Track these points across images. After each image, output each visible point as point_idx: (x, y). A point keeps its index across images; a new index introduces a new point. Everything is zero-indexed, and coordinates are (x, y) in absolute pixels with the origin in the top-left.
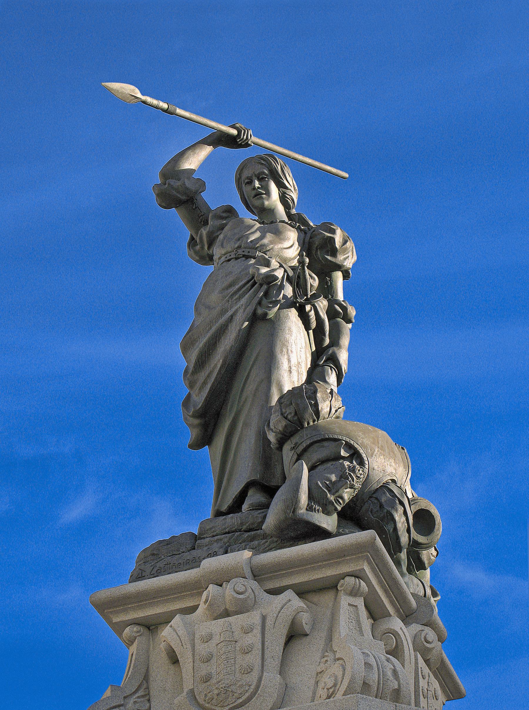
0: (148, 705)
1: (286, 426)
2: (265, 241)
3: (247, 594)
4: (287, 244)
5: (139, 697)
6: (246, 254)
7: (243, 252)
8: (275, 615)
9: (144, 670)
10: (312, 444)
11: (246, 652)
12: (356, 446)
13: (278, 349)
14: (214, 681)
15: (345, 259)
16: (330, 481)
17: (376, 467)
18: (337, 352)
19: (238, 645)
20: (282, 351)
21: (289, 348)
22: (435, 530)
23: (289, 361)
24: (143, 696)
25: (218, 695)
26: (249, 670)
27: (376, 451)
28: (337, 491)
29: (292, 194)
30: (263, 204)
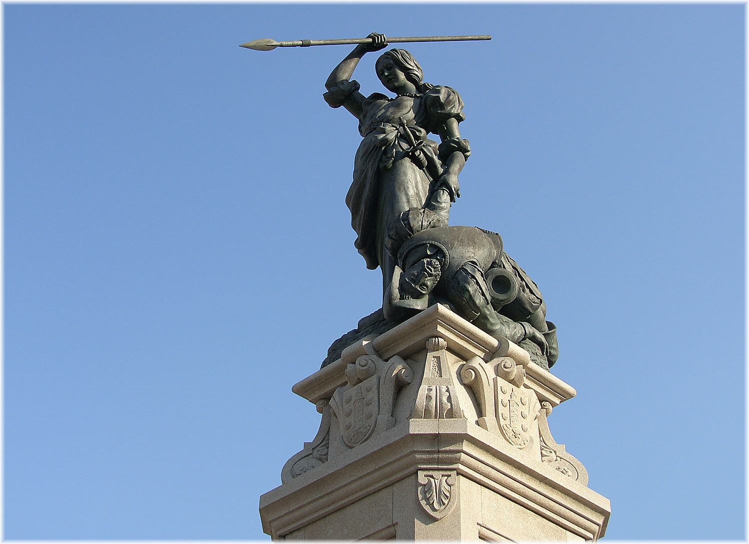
0: (327, 450)
1: (392, 244)
2: (388, 114)
4: (405, 111)
5: (322, 447)
7: (374, 126)
8: (384, 376)
10: (409, 252)
12: (439, 245)
13: (397, 189)
15: (452, 108)
16: (414, 275)
17: (455, 256)
18: (446, 177)
20: (400, 189)
21: (406, 186)
22: (511, 288)
23: (407, 195)
24: (324, 446)
25: (354, 436)
26: (369, 417)
27: (456, 244)
28: (419, 281)
29: (416, 73)
30: (395, 85)
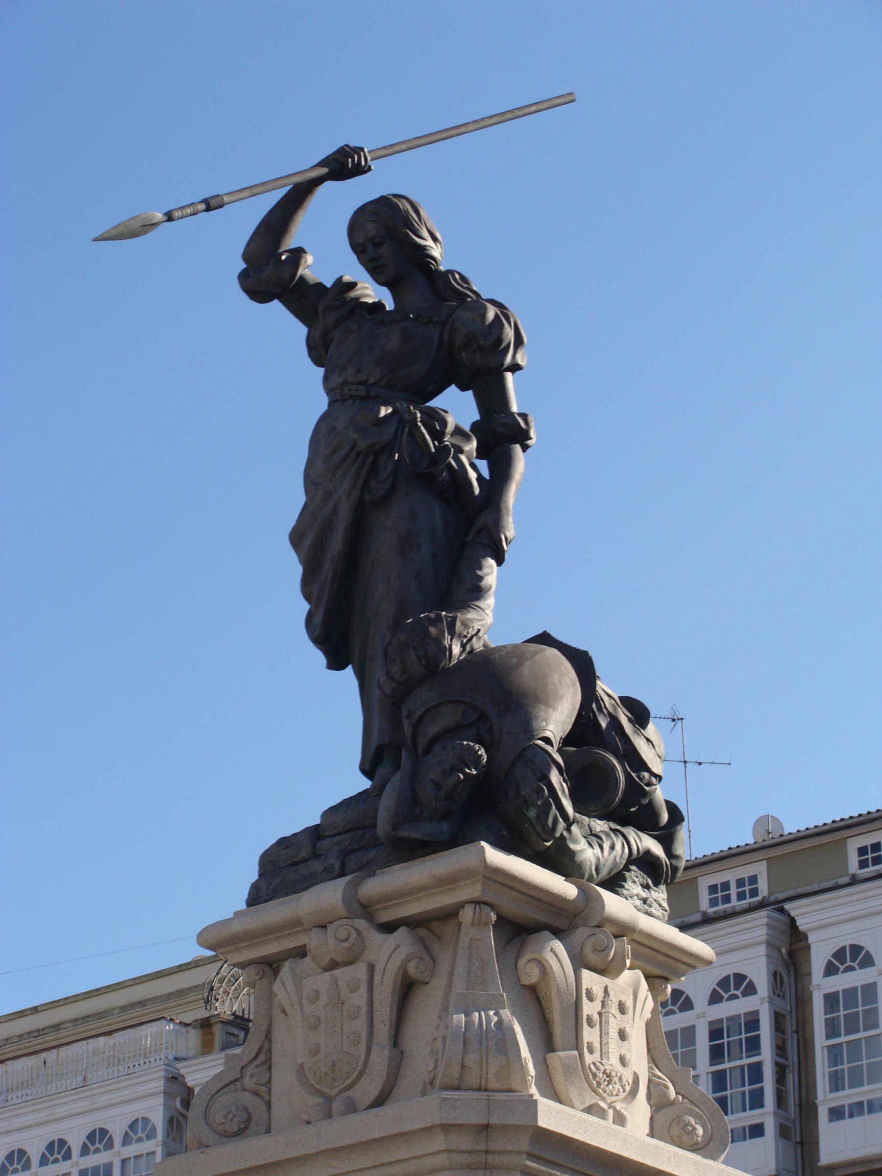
0: (268, 1075)
3: (351, 940)
6: (353, 393)
9: (265, 1026)
11: (353, 1018)
14: (321, 1055)
19: (345, 1007)
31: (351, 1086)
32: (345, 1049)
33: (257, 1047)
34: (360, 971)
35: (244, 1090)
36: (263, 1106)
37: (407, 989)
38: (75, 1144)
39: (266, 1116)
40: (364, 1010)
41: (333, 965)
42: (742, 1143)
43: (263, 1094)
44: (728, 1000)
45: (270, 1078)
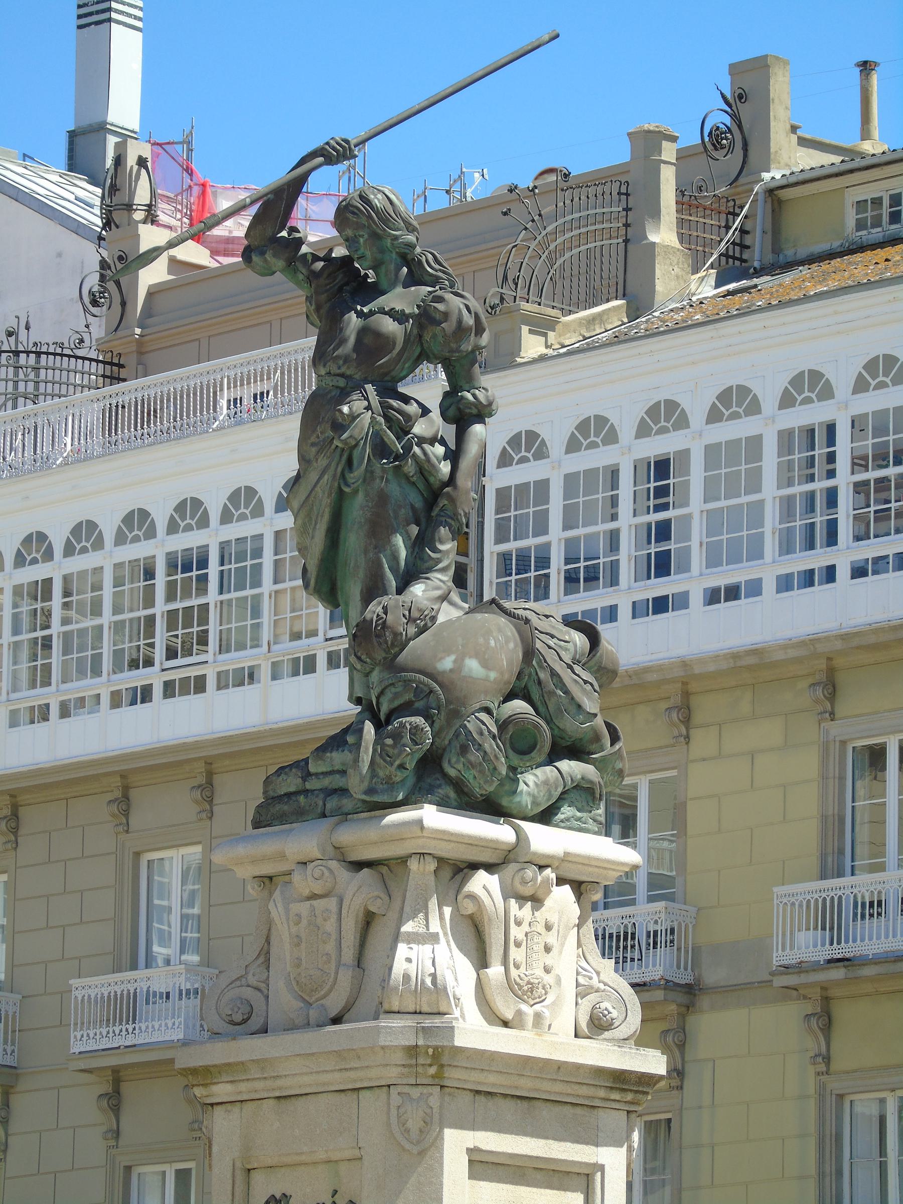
31: (324, 997)
32: (320, 966)
33: (259, 949)
34: (331, 904)
35: (248, 986)
36: (263, 999)
37: (368, 920)
38: (161, 517)
39: (265, 1008)
40: (334, 936)
41: (313, 897)
42: (646, 619)
43: (263, 989)
44: (657, 433)
45: (268, 977)
